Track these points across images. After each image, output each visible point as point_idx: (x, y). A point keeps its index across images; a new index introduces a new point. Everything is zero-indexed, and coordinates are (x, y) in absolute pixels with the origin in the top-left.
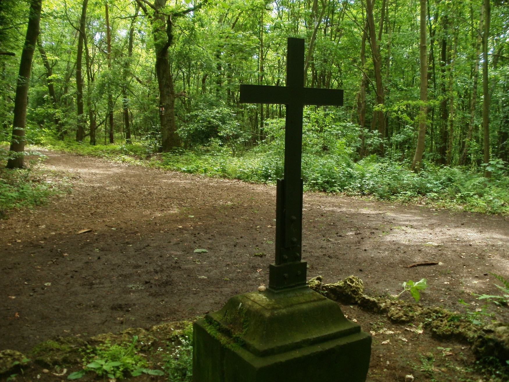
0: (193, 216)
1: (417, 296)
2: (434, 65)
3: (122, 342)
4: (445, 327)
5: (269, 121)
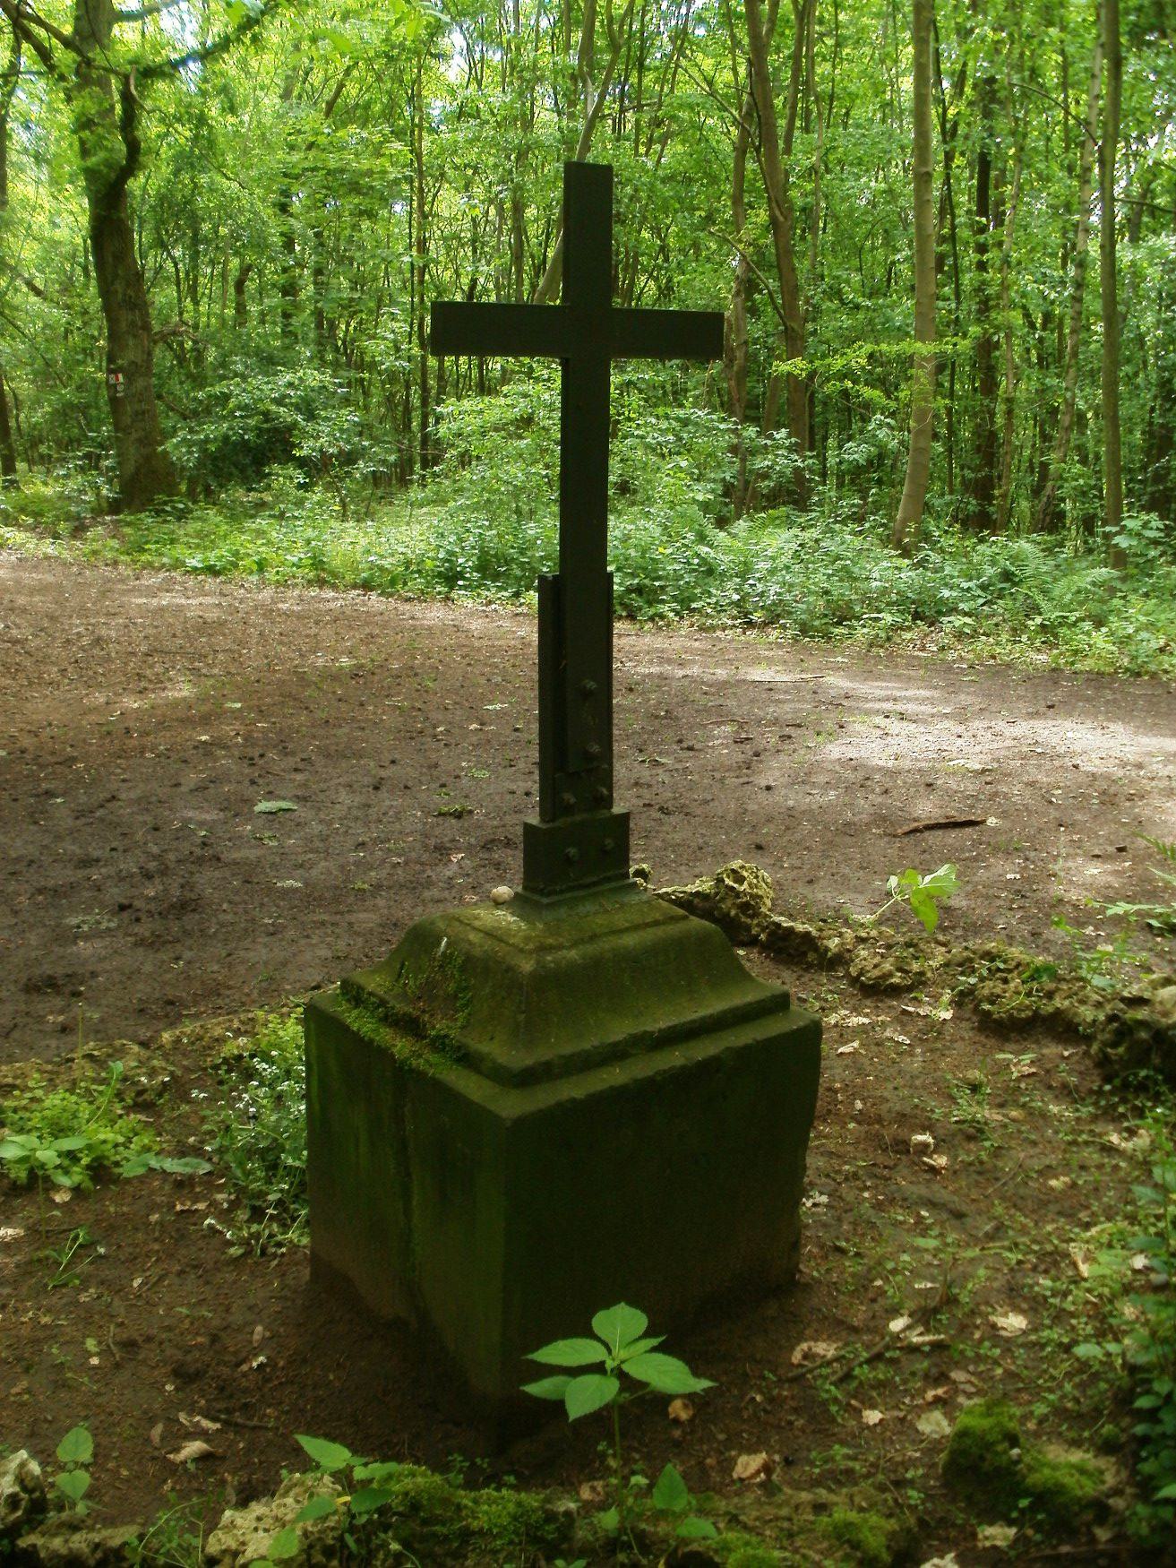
0: (239, 705)
1: (931, 917)
2: (953, 227)
3: (74, 1083)
4: (1014, 997)
5: (448, 407)
